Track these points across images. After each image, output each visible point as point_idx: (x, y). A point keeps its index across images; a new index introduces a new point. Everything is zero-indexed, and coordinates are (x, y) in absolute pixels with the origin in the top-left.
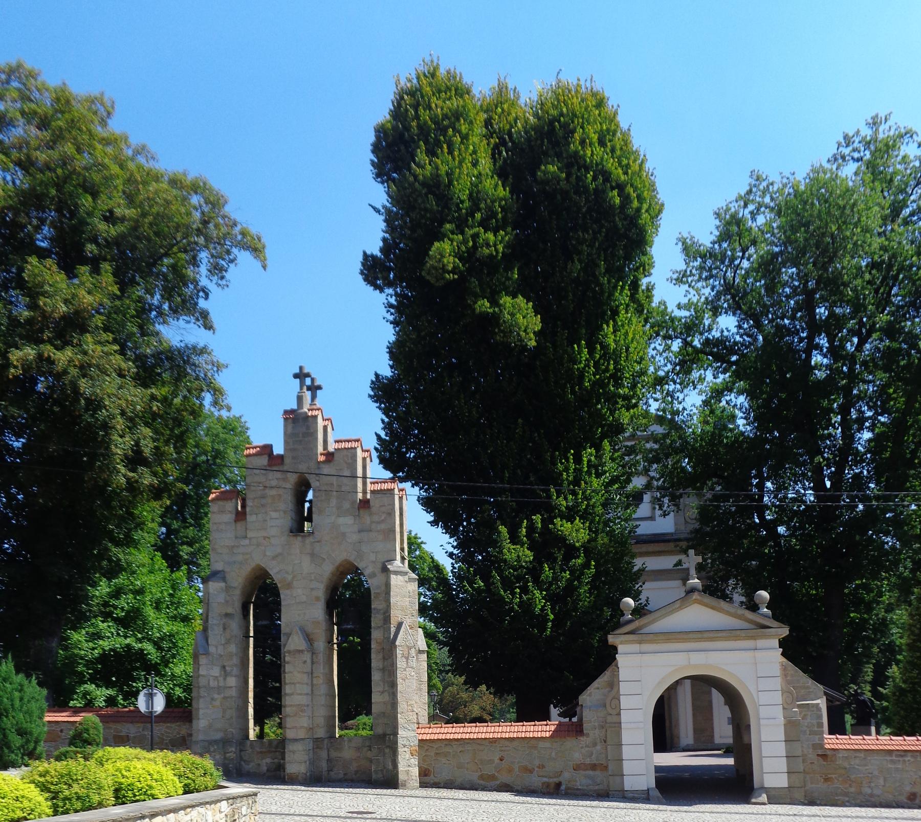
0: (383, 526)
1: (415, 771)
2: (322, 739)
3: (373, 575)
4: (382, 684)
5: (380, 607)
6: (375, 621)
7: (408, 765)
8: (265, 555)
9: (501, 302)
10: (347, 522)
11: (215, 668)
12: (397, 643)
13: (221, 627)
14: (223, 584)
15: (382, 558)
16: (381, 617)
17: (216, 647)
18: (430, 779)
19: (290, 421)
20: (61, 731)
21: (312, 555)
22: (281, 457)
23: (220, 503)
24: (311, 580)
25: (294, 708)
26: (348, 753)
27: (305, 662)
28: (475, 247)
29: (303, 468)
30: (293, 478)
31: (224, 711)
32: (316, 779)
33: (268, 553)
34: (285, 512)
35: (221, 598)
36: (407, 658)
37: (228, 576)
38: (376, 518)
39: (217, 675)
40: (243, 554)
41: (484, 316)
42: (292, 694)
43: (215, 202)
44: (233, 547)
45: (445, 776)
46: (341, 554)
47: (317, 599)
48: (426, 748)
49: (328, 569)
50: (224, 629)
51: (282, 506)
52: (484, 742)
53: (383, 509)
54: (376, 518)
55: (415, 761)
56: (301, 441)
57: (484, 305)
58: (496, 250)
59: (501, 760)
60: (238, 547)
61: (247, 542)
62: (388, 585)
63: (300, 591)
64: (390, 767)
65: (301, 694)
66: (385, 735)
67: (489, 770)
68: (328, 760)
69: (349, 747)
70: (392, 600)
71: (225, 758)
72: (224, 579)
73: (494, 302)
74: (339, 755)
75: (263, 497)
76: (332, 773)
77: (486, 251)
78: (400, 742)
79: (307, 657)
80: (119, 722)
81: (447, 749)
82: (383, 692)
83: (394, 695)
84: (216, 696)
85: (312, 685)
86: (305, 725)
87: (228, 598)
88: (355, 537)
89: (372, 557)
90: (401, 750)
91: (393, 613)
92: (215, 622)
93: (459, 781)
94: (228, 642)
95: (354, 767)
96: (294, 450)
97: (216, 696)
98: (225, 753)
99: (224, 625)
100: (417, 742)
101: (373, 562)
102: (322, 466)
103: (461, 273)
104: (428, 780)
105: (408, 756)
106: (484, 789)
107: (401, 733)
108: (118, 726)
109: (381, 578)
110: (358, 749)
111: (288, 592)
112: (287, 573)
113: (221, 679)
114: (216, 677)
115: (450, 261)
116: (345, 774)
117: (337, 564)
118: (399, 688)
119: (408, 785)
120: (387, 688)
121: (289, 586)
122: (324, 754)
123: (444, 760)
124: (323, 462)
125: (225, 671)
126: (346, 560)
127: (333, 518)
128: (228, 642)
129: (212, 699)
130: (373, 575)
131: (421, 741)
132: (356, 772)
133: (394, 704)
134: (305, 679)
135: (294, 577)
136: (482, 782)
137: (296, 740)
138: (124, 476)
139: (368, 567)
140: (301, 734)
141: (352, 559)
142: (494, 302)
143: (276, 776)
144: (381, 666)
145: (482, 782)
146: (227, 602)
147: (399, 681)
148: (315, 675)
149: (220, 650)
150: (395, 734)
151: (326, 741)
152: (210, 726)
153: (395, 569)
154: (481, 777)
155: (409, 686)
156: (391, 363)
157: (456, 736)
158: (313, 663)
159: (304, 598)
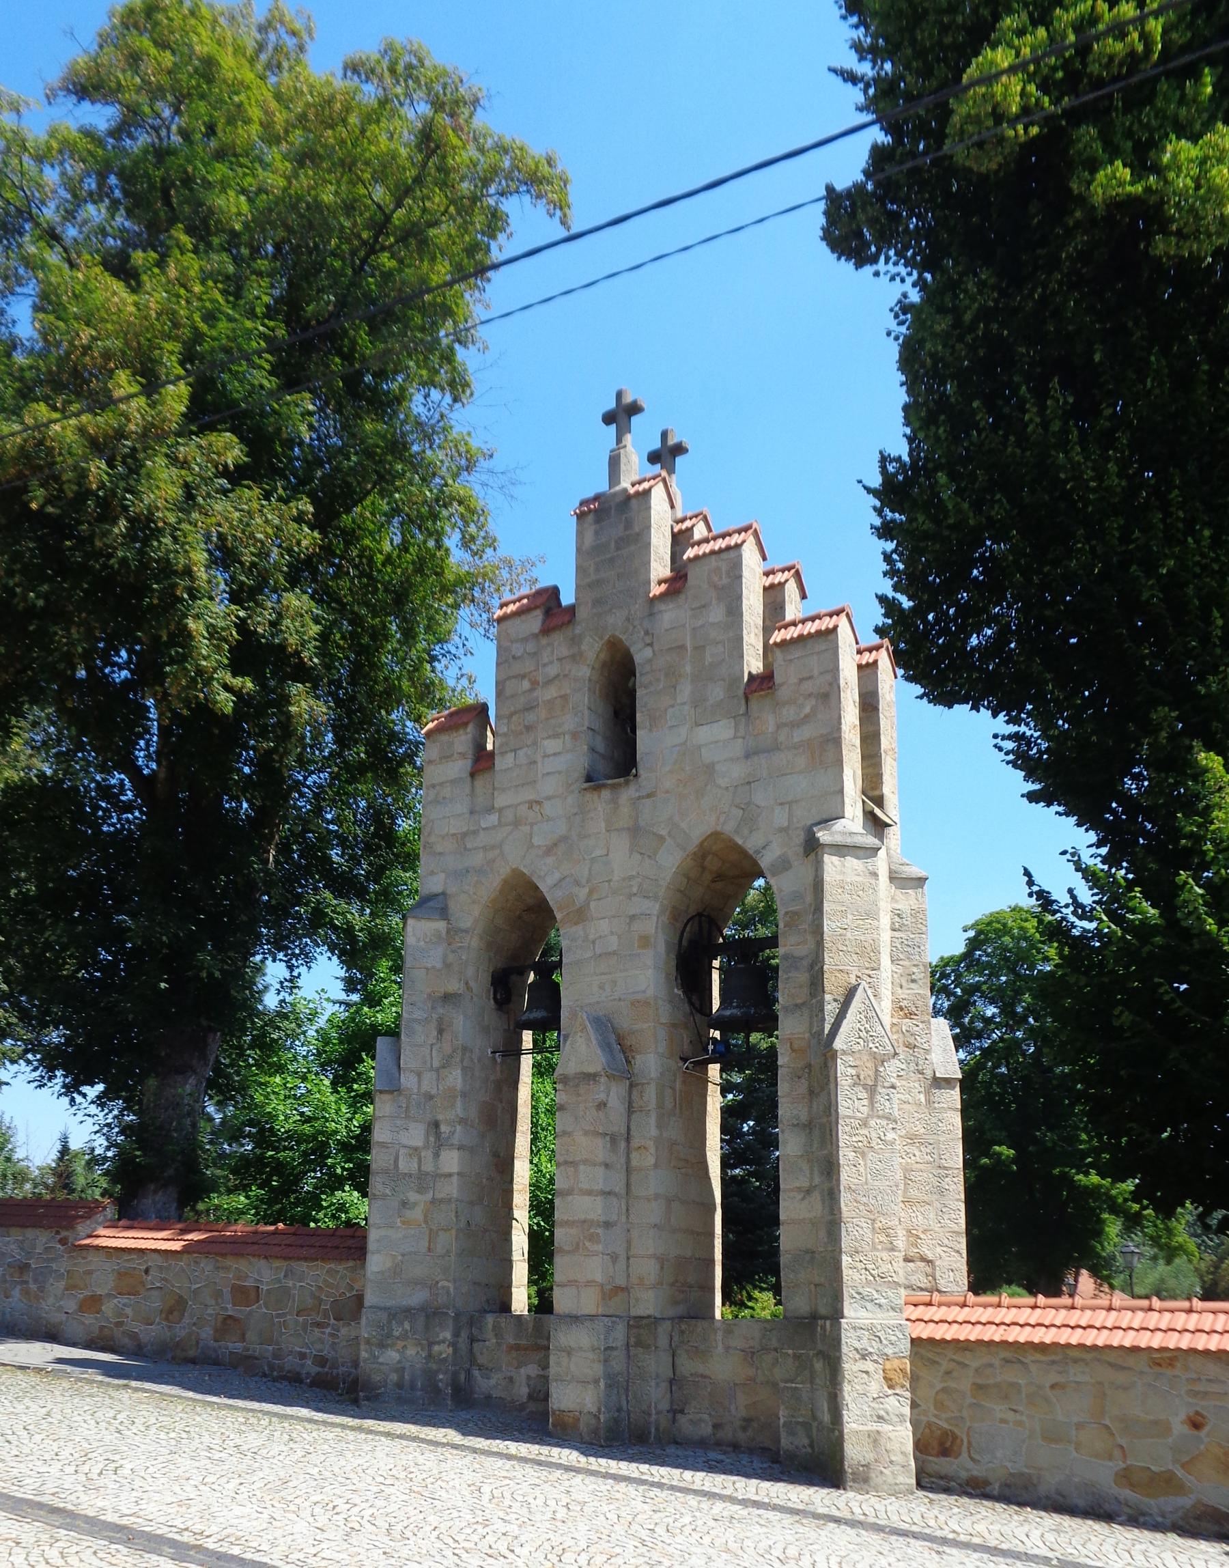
0: (806, 732)
1: (902, 1438)
2: (652, 1322)
3: (783, 865)
4: (805, 1167)
5: (802, 950)
6: (787, 993)
7: (876, 1415)
8: (531, 846)
9: (1166, 158)
10: (717, 737)
11: (412, 1125)
12: (838, 1044)
13: (434, 1025)
14: (441, 925)
15: (804, 816)
16: (803, 977)
17: (419, 1075)
18: (959, 1466)
19: (591, 518)
20: (147, 1271)
21: (635, 831)
22: (572, 609)
23: (444, 738)
24: (630, 896)
25: (574, 1231)
26: (722, 1366)
27: (602, 1105)
28: (1083, 50)
29: (615, 622)
30: (592, 649)
31: (433, 1235)
32: (632, 1434)
33: (536, 841)
34: (575, 735)
35: (434, 958)
36: (872, 1091)
37: (453, 906)
38: (789, 713)
39: (420, 1144)
40: (484, 848)
41: (1123, 206)
42: (569, 1192)
43: (451, 102)
44: (465, 835)
45: (1001, 1461)
46: (699, 823)
47: (645, 941)
48: (945, 1365)
49: (670, 862)
50: (441, 1031)
51: (569, 722)
52: (1131, 1361)
53: (807, 687)
54: (789, 713)
55: (899, 1405)
56: (611, 561)
57: (1116, 178)
58: (1145, 37)
59: (1196, 1425)
60: (475, 832)
61: (493, 819)
62: (818, 886)
63: (604, 926)
64: (826, 1418)
65: (589, 1193)
66: (814, 1317)
67: (1152, 1456)
68: (671, 1382)
69: (727, 1349)
70: (828, 926)
71: (430, 1356)
72: (444, 913)
73: (1143, 163)
74: (701, 1369)
75: (530, 708)
76: (682, 1420)
77: (1116, 47)
78: (850, 1341)
79: (615, 1095)
80: (242, 1255)
81: (1011, 1375)
82: (808, 1192)
83: (832, 1196)
84: (413, 1197)
85: (629, 1170)
86: (599, 1277)
87: (451, 957)
88: (738, 771)
89: (780, 818)
90: (850, 1366)
91: (830, 961)
92: (418, 1014)
93: (1050, 1482)
94: (446, 1064)
95: (739, 1407)
96: (599, 583)
97: (413, 1197)
98: (431, 1344)
99: (440, 1021)
100: (905, 1346)
101: (784, 830)
102: (661, 606)
103: (1048, 120)
104: (943, 1466)
105: (876, 1385)
106: (1137, 1519)
107: (853, 1313)
108: (242, 1265)
109: (801, 872)
110: (750, 1355)
111: (578, 930)
112: (577, 883)
113: (427, 1155)
114: (416, 1149)
115: (1013, 92)
116: (716, 1426)
117: (692, 846)
118: (847, 1176)
119: (876, 1479)
120: (817, 1180)
121: (580, 915)
122: (655, 1364)
123: (999, 1409)
124: (663, 596)
125: (438, 1134)
126: (716, 835)
127: (683, 731)
128: (446, 1064)
129: (404, 1204)
130: (783, 865)
131: (916, 1342)
132: (748, 1421)
133: (833, 1225)
134: (598, 1149)
135: (591, 892)
136: (1126, 1493)
137: (574, 1319)
138: (227, 688)
139: (768, 844)
140: (589, 1303)
141: (729, 828)
142: (1143, 163)
143: (532, 1420)
144: (804, 1117)
145: (1126, 1493)
146: (447, 965)
147: (846, 1155)
148: (635, 1143)
149: (428, 1084)
150: (837, 1314)
151: (664, 1329)
152: (396, 1271)
153: (839, 839)
154: (1126, 1477)
155: (877, 1174)
156: (908, 431)
157: (1039, 1336)
158: (630, 1110)
159: (613, 943)
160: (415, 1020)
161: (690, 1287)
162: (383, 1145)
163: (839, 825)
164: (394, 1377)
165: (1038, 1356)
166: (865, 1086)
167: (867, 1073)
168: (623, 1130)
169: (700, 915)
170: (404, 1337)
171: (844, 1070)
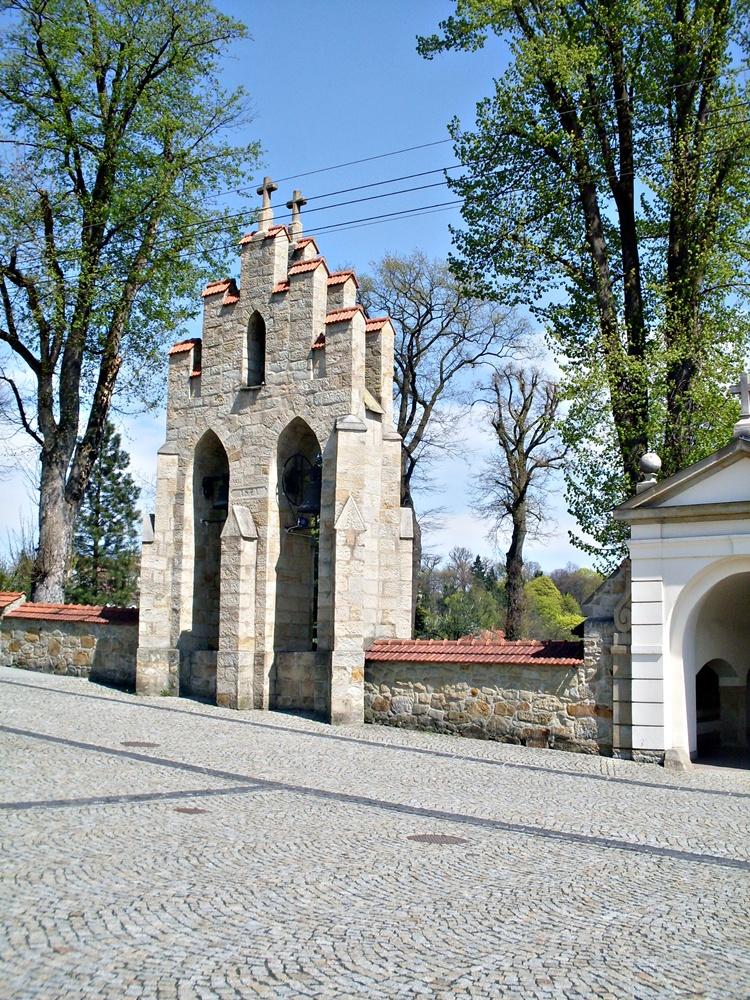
36: (353, 548)
69: (299, 666)
74: (289, 676)
132: (306, 699)
147: (339, 578)
153: (346, 426)
160: (162, 506)
161: (290, 637)
162: (146, 569)
163: (349, 419)
164: (152, 681)
165: (420, 666)
166: (349, 546)
167: (351, 539)
168: (254, 563)
169: (295, 456)
170: (157, 661)
171: (340, 538)
